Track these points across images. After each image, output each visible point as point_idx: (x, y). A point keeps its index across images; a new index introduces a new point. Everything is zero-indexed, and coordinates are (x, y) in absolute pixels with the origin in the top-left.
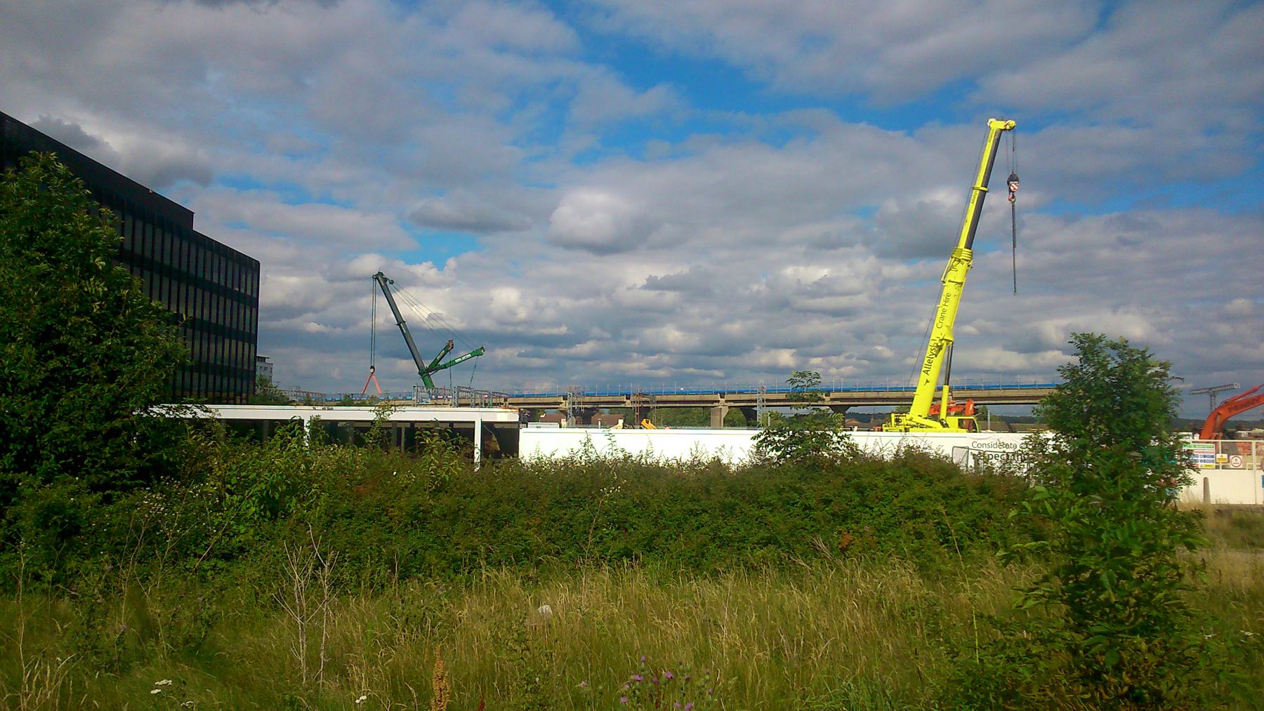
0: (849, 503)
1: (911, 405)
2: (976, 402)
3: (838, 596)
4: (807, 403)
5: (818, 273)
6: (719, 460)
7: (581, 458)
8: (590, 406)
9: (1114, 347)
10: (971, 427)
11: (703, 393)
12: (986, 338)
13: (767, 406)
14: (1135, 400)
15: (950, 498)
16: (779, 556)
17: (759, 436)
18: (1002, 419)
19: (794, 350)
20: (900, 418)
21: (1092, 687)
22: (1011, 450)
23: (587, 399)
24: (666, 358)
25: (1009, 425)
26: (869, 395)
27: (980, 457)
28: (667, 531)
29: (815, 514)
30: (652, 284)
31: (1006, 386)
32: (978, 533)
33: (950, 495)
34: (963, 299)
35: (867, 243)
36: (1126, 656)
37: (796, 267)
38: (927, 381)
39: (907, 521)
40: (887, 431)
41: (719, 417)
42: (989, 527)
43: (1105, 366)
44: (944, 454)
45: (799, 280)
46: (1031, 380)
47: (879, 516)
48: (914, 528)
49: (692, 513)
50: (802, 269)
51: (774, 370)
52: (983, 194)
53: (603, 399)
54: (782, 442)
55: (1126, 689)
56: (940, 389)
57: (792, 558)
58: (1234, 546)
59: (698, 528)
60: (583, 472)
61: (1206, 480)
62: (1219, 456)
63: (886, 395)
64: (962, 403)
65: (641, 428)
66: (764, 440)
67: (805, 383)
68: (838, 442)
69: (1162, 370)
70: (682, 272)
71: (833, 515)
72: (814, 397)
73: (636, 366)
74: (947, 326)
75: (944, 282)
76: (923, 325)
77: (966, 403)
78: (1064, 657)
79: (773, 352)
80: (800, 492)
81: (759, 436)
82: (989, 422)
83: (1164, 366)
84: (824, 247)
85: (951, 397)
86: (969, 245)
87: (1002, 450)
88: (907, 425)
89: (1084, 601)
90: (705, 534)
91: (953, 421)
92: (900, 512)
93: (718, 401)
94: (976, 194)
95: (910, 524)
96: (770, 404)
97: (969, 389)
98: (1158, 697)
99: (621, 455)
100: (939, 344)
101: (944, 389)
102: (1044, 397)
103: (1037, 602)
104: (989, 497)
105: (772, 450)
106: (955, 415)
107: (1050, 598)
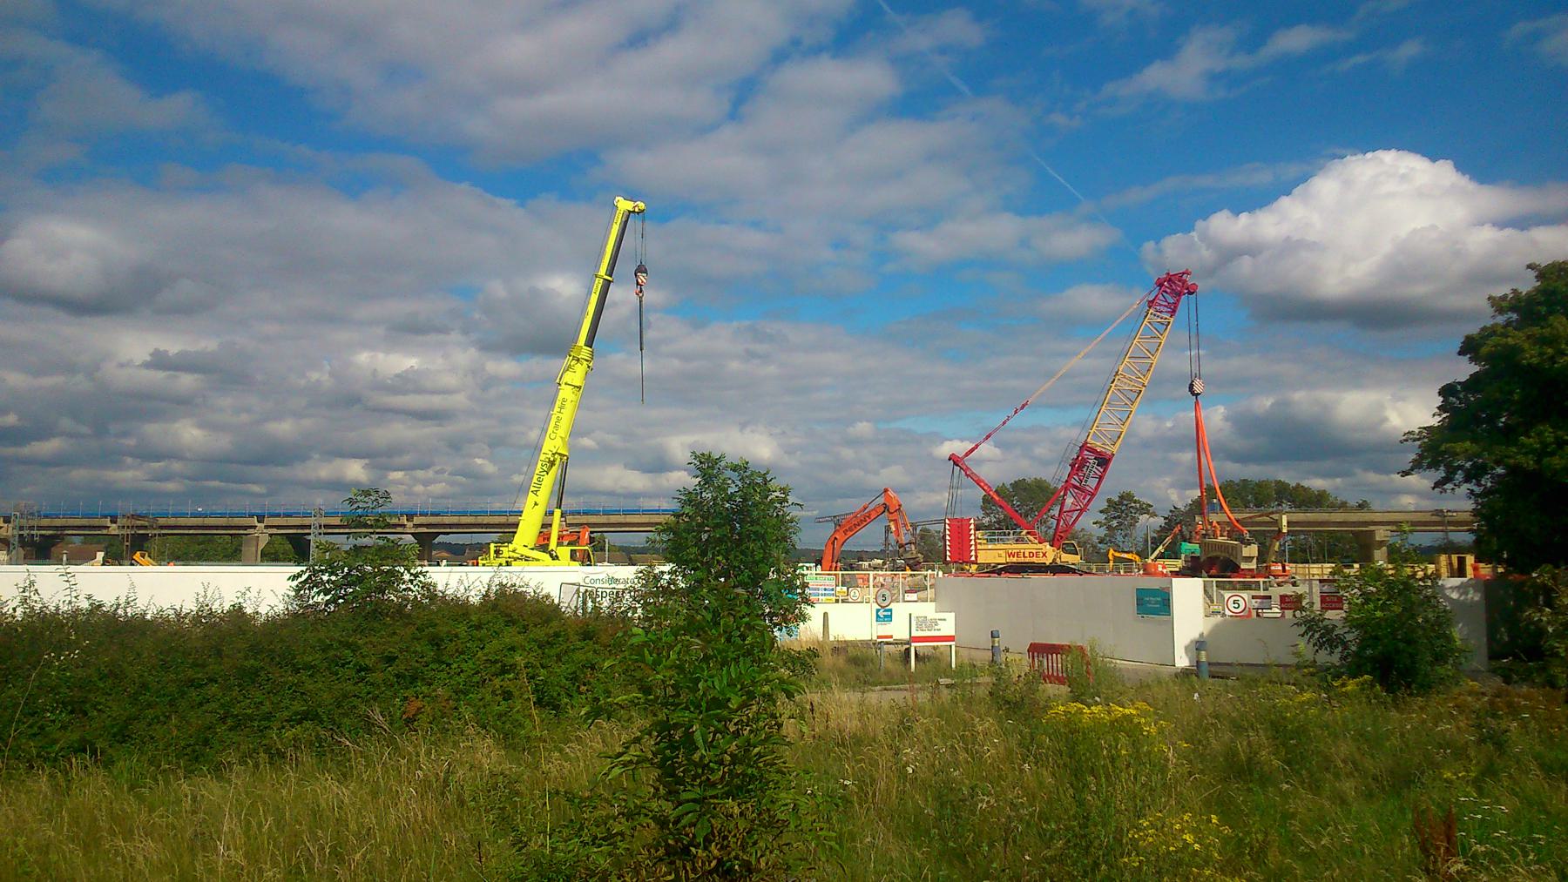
0: (420, 660)
1: (515, 533)
2: (593, 530)
3: (392, 782)
4: (371, 530)
5: (403, 362)
6: (241, 608)
7: (14, 609)
8: (51, 532)
9: (735, 469)
10: (586, 560)
11: (232, 516)
12: (606, 454)
13: (325, 534)
14: (757, 528)
15: (548, 646)
16: (317, 736)
17: (299, 575)
18: (622, 549)
19: (367, 461)
20: (501, 549)
21: (679, 863)
22: (622, 586)
23: (45, 522)
24: (177, 466)
25: (627, 556)
26: (464, 520)
27: (590, 594)
28: (151, 711)
29: (371, 677)
30: (159, 361)
31: (628, 510)
32: (579, 687)
33: (548, 643)
34: (580, 406)
35: (466, 331)
36: (716, 823)
37: (372, 354)
38: (536, 504)
39: (494, 678)
40: (484, 565)
41: (254, 549)
42: (591, 680)
43: (725, 490)
44: (544, 593)
45: (375, 370)
46: (654, 504)
47: (459, 674)
48: (501, 686)
49: (192, 683)
50: (381, 356)
51: (337, 485)
52: (607, 284)
53: (71, 522)
54: (333, 582)
55: (714, 863)
56: (552, 513)
57: (336, 737)
58: (844, 685)
59: (201, 704)
60: (17, 630)
61: (825, 615)
62: (838, 589)
63: (486, 520)
64: (577, 530)
65: (132, 565)
66: (306, 580)
67: (370, 504)
68: (411, 581)
69: (783, 496)
70: (206, 347)
71: (397, 676)
72: (382, 523)
73: (129, 476)
74: (561, 437)
75: (560, 384)
76: (533, 435)
77: (581, 530)
78: (651, 832)
79: (338, 462)
80: (354, 648)
81: (299, 575)
82: (607, 553)
83: (783, 490)
84: (409, 331)
85: (564, 523)
86: (589, 343)
87: (611, 586)
88: (509, 557)
89: (677, 762)
90: (211, 712)
91: (564, 552)
92: (485, 667)
93: (255, 527)
94: (599, 284)
95: (497, 682)
96: (330, 531)
97: (586, 513)
98: (748, 868)
99: (85, 605)
100: (552, 459)
101: (555, 514)
102: (660, 524)
103: (623, 770)
104: (594, 643)
105: (318, 593)
106: (569, 544)
107: (637, 763)
